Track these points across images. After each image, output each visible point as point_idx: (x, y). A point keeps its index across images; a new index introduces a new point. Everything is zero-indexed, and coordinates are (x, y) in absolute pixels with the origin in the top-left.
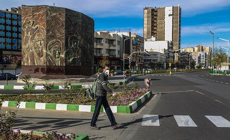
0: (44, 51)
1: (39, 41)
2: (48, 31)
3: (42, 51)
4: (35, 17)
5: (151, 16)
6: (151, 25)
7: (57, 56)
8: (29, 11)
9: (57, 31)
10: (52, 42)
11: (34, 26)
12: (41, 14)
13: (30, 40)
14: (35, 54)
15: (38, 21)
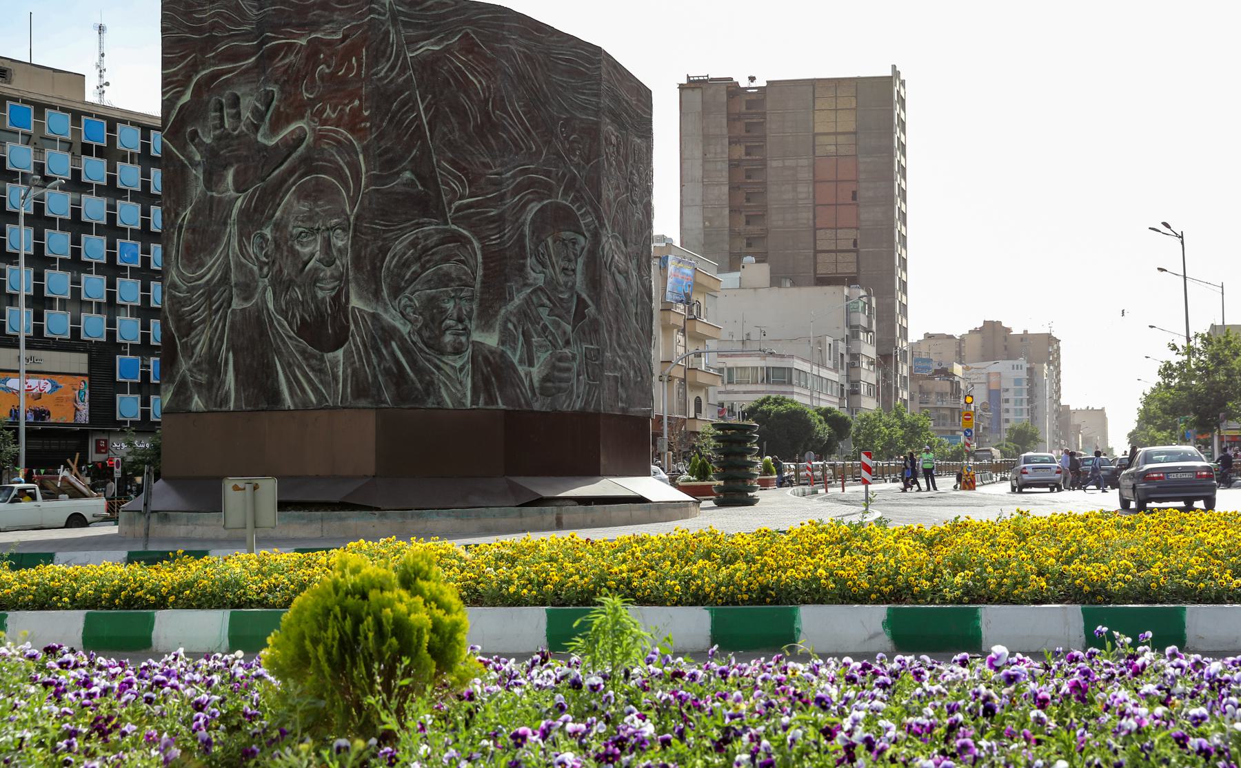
0: (355, 302)
1: (313, 231)
2: (388, 164)
3: (339, 302)
4: (279, 63)
5: (725, 131)
6: (726, 189)
7: (448, 338)
8: (228, 19)
9: (453, 163)
10: (413, 244)
11: (274, 129)
12: (330, 43)
13: (233, 229)
14: (284, 328)
15: (306, 95)
